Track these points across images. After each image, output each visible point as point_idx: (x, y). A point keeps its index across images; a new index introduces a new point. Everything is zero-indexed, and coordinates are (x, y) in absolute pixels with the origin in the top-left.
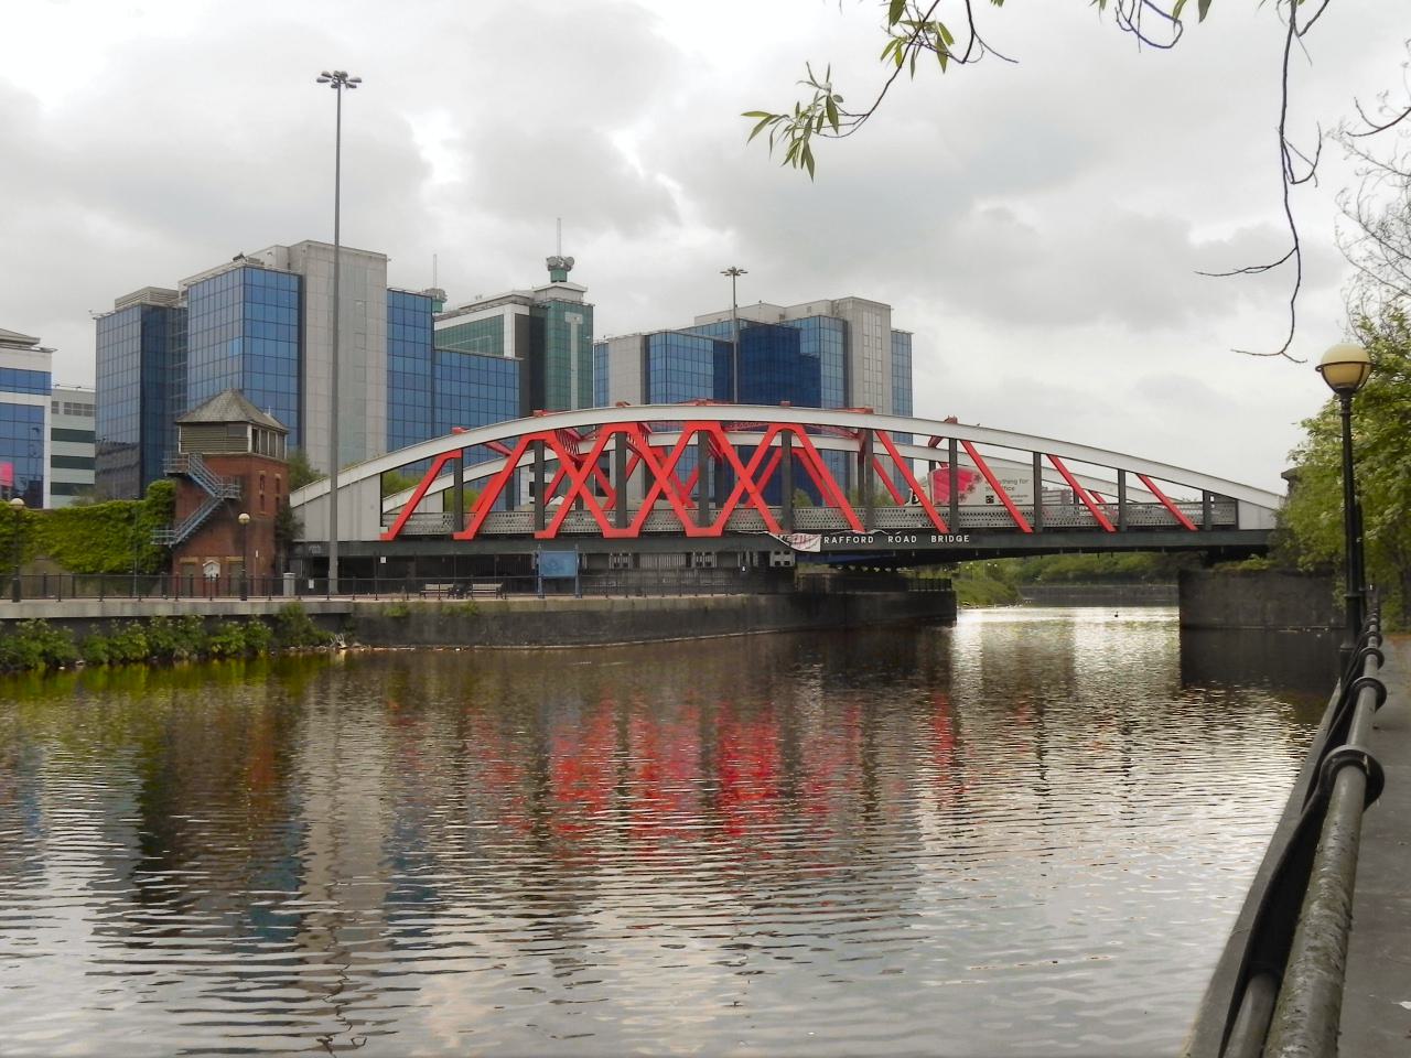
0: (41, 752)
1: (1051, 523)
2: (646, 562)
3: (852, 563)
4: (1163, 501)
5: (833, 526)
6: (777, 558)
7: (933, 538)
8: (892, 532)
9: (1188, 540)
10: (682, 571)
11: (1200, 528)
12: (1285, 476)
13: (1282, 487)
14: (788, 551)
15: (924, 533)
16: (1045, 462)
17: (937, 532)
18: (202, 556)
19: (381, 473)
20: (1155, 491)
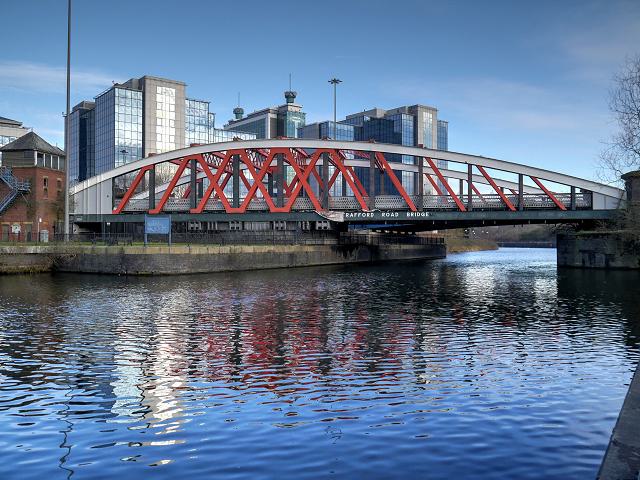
0: (140, 265)
1: (527, 205)
2: (247, 226)
3: (387, 228)
4: (547, 192)
5: (352, 207)
6: (192, 225)
7: (408, 214)
8: (385, 210)
9: (560, 215)
10: (267, 231)
11: (569, 209)
12: (623, 177)
13: (621, 185)
14: (326, 220)
15: (456, 209)
16: (475, 170)
17: (410, 210)
18: (12, 222)
19: (114, 178)
20: (542, 188)
